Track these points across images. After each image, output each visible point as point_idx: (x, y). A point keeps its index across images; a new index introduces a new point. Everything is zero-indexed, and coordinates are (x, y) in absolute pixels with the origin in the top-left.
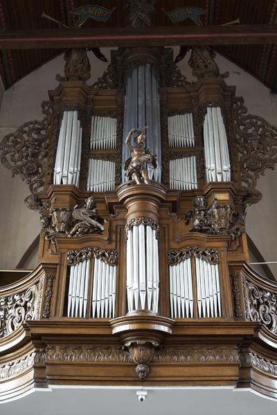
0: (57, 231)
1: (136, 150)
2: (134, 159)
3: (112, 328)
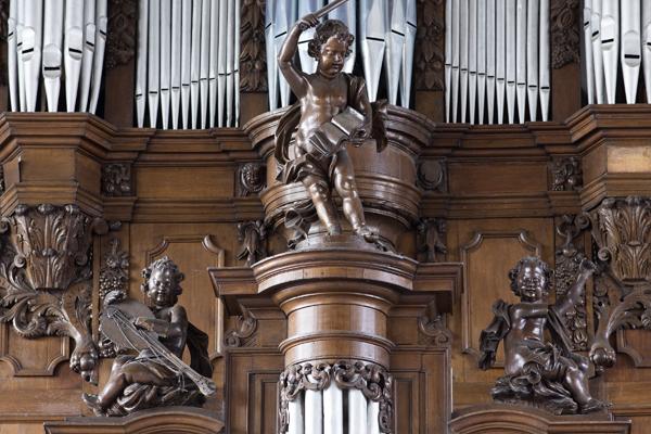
0: (34, 286)
2: (308, 126)
3: (256, 284)
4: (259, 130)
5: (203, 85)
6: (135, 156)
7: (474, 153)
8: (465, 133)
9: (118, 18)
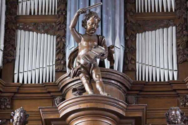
1: (85, 40)
2: (82, 53)
3: (59, 114)
4: (62, 82)
5: (41, 70)
6: (12, 94)
7: (148, 93)
8: (145, 84)
9: (8, 45)
